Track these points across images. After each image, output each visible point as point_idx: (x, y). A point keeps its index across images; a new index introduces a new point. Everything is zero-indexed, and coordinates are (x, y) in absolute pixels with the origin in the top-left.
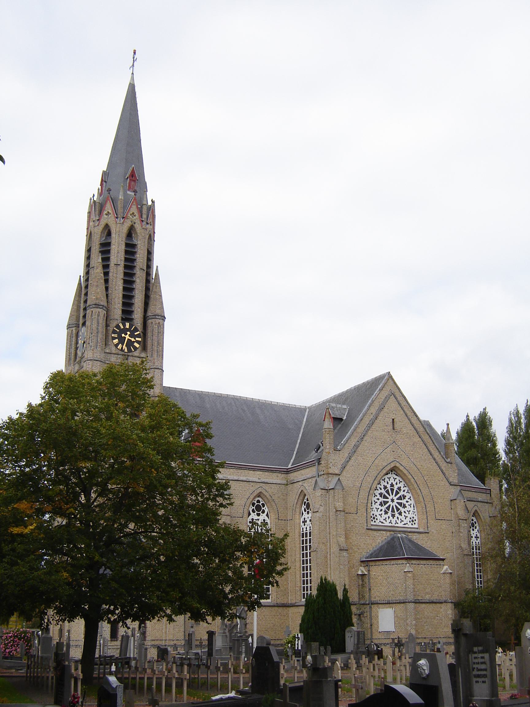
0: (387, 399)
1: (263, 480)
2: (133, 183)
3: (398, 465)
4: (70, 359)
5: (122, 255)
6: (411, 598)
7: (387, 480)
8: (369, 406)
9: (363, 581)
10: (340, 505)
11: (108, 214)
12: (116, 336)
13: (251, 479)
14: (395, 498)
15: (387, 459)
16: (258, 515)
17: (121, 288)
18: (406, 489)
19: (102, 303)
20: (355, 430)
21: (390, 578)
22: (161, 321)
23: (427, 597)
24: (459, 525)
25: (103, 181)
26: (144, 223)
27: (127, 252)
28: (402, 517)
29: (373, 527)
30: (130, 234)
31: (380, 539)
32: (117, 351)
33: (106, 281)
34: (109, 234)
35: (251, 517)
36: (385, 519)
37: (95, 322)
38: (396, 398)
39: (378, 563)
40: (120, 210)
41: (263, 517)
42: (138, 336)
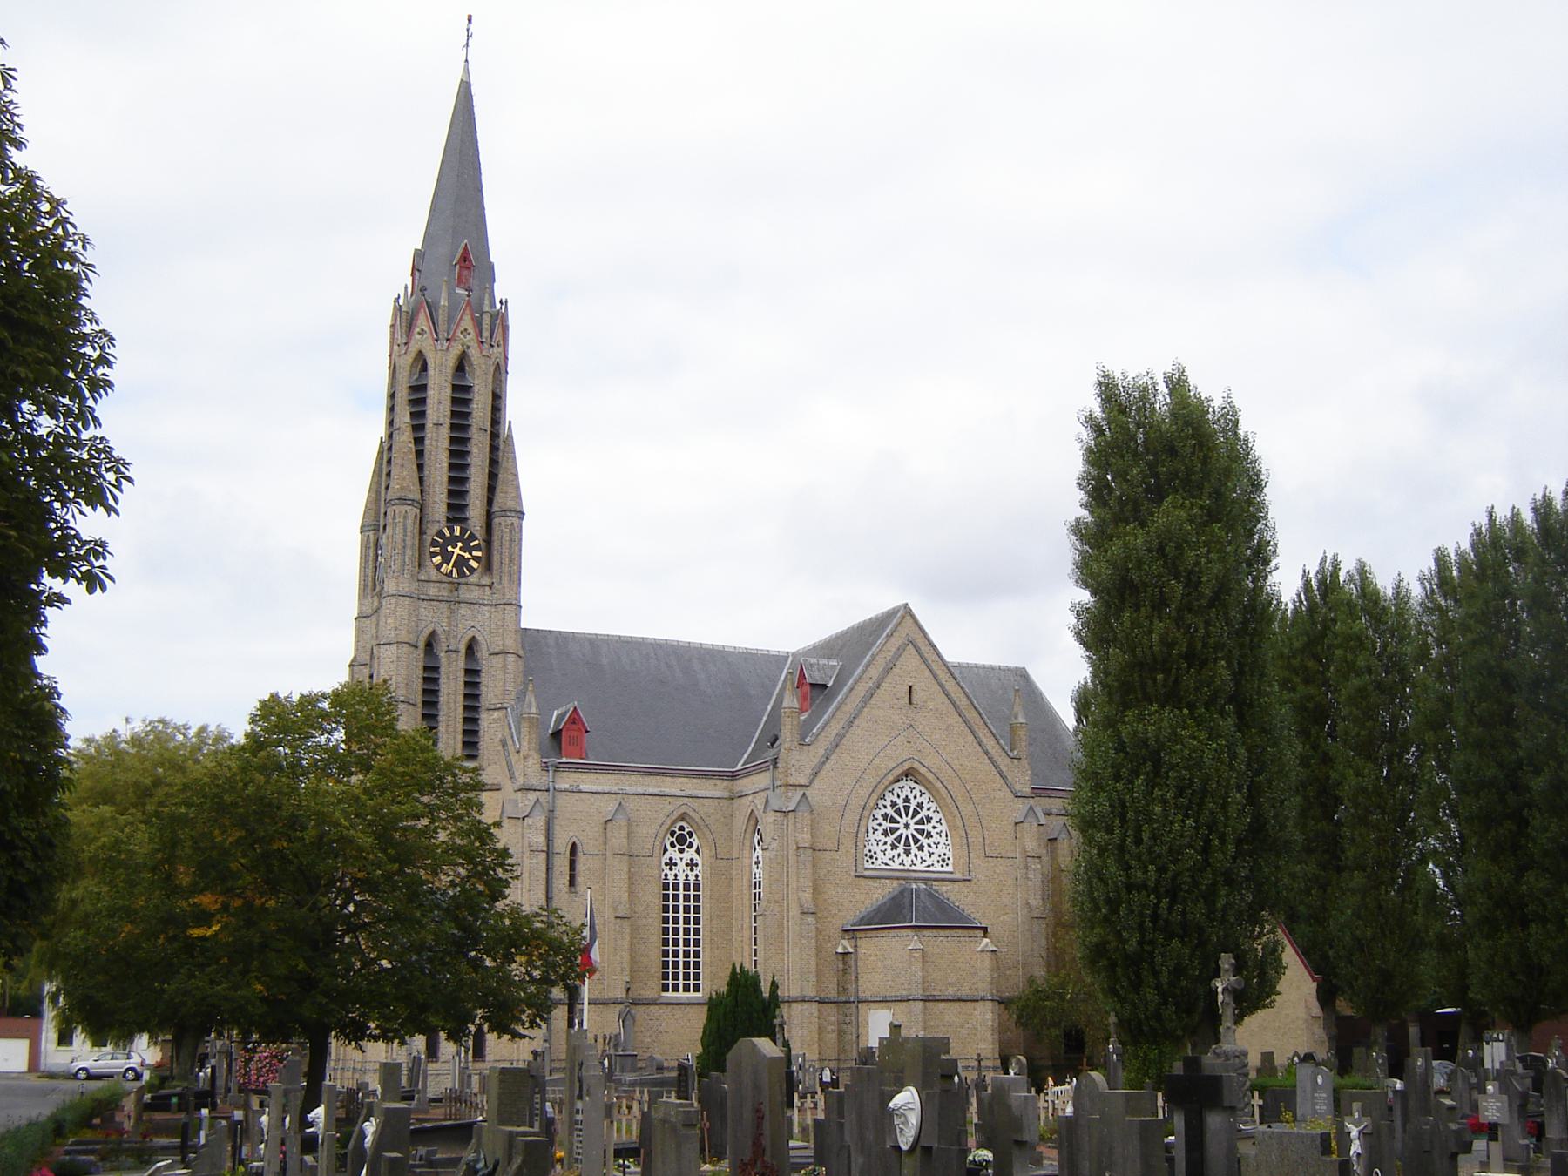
0: (900, 652)
1: (689, 792)
2: (465, 272)
3: (916, 765)
4: (365, 586)
5: (446, 407)
6: (918, 993)
7: (897, 791)
8: (867, 666)
9: (845, 963)
10: (805, 838)
11: (422, 332)
12: (437, 550)
13: (667, 791)
14: (912, 822)
15: (898, 755)
16: (681, 851)
17: (446, 465)
18: (933, 806)
19: (411, 496)
20: (838, 708)
21: (889, 960)
22: (515, 520)
23: (951, 992)
24: (1026, 867)
25: (415, 270)
26: (486, 346)
27: (455, 401)
28: (925, 855)
29: (867, 873)
30: (461, 367)
31: (879, 894)
32: (440, 577)
33: (420, 454)
34: (425, 368)
35: (667, 855)
36: (892, 859)
37: (399, 529)
38: (917, 649)
39: (869, 934)
40: (442, 327)
41: (690, 854)
42: (477, 548)
